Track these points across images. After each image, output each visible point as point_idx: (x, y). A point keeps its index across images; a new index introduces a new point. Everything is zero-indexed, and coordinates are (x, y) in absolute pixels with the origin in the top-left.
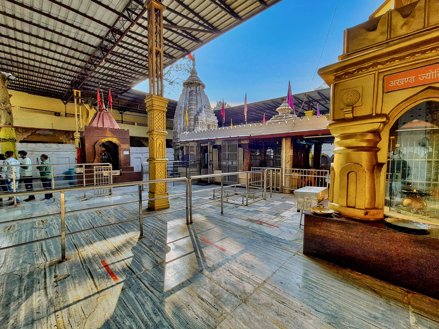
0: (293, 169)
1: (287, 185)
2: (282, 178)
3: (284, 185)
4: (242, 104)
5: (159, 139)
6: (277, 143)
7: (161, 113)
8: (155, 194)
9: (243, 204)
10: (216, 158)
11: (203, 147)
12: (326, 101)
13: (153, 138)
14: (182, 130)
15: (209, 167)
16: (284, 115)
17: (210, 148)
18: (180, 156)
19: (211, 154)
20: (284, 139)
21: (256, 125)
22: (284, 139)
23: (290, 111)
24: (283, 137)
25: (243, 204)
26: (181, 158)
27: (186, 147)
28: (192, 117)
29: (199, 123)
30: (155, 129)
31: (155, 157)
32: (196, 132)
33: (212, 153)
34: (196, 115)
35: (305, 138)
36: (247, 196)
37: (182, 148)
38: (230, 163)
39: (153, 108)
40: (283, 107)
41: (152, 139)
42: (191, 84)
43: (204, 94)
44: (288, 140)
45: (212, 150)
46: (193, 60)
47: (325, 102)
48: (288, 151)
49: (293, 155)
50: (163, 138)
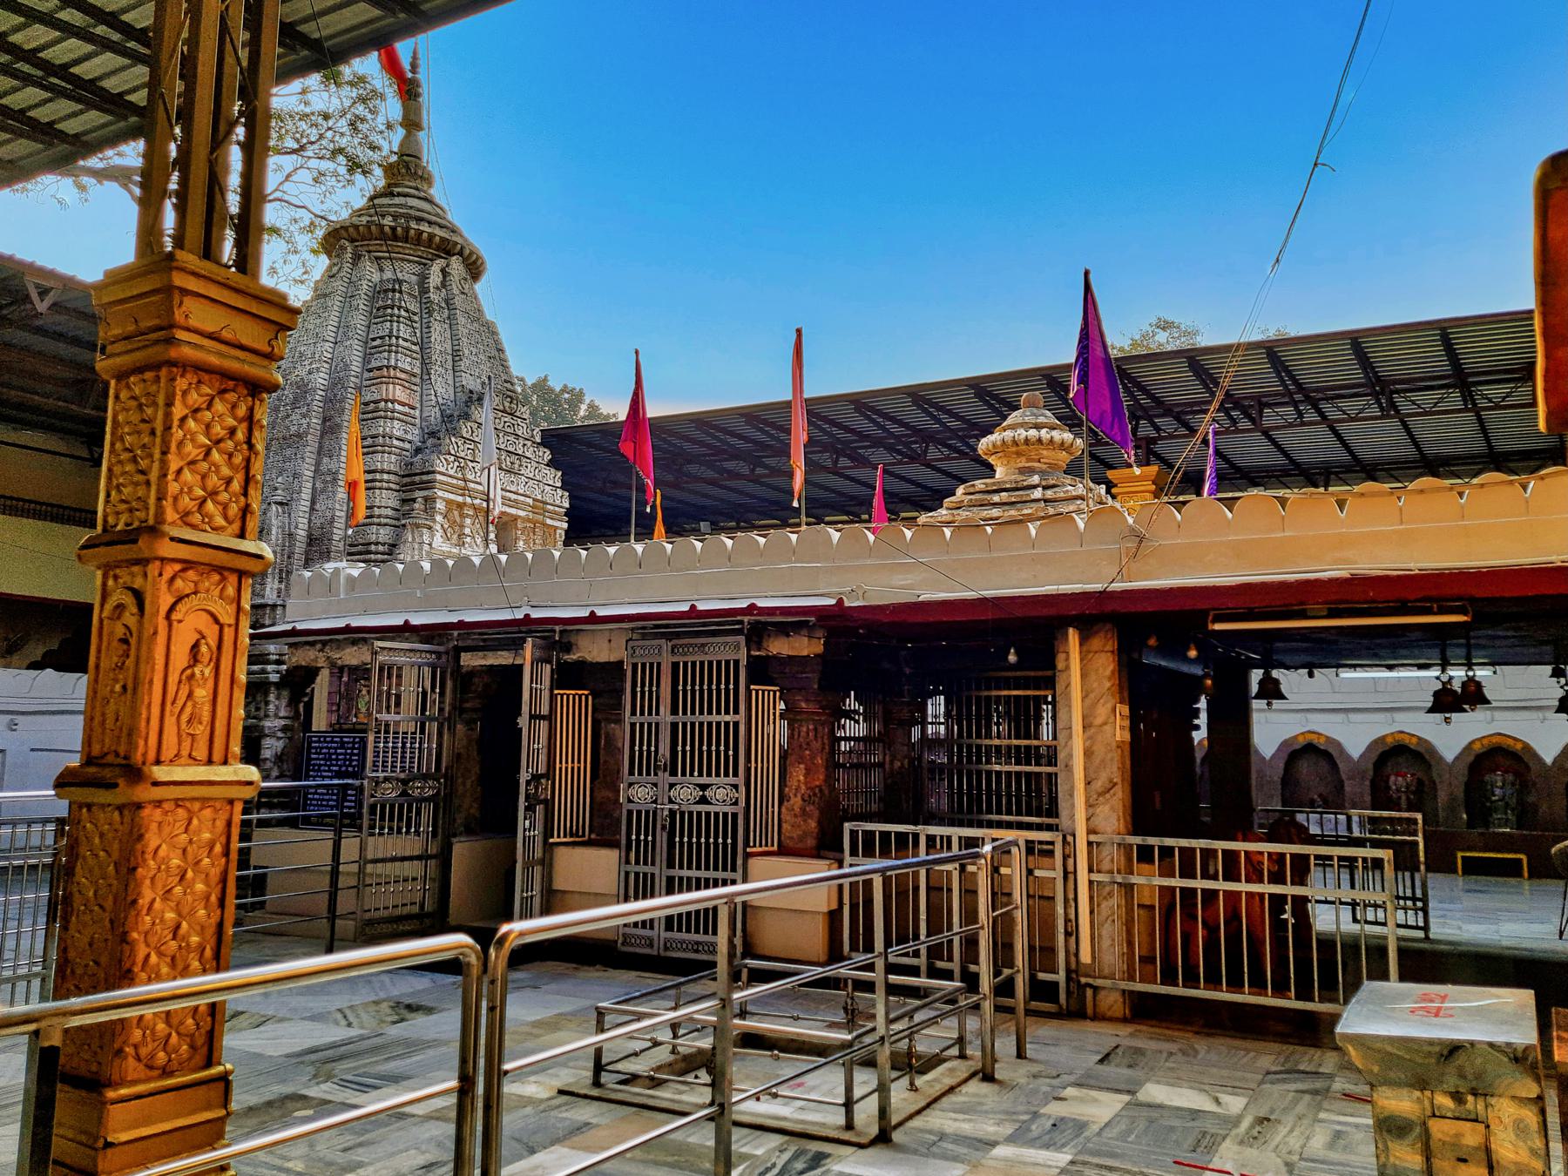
0: (1138, 840)
1: (1113, 957)
2: (1071, 900)
3: (1085, 957)
4: (776, 390)
5: (194, 601)
6: (1012, 658)
7: (232, 397)
8: (111, 1094)
9: (849, 1126)
10: (574, 764)
11: (474, 672)
12: (1231, 418)
13: (139, 596)
14: (300, 547)
15: (522, 823)
16: (1036, 479)
17: (535, 685)
18: (267, 742)
19: (544, 725)
20: (1073, 636)
21: (871, 537)
22: (1073, 636)
23: (1064, 458)
24: (1062, 623)
25: (849, 1126)
26: (279, 759)
27: (338, 670)
28: (388, 462)
29: (440, 505)
30: (171, 515)
31: (144, 748)
32: (427, 566)
33: (550, 718)
34: (418, 451)
35: (1218, 627)
36: (884, 1055)
37: (298, 682)
38: (685, 794)
39: (173, 353)
40: (1008, 434)
41: (129, 600)
42: (382, 236)
43: (476, 316)
44: (1096, 643)
45: (552, 698)
46: (408, 90)
47: (1227, 424)
48: (1102, 712)
49: (1131, 743)
50: (231, 591)
